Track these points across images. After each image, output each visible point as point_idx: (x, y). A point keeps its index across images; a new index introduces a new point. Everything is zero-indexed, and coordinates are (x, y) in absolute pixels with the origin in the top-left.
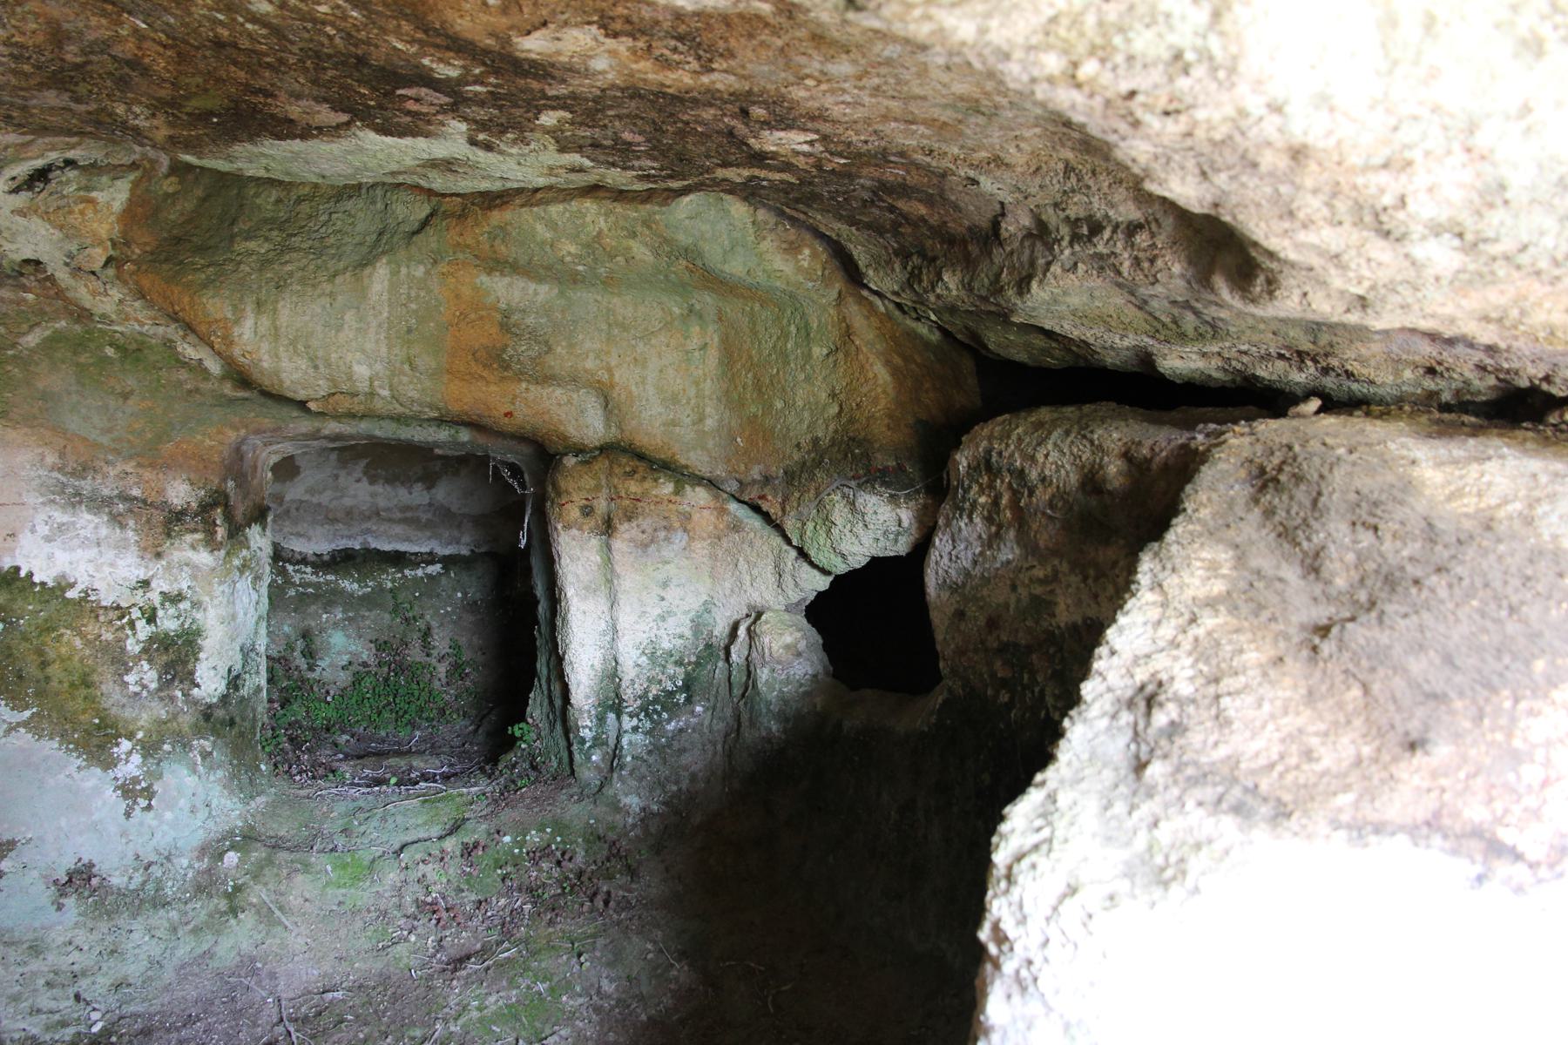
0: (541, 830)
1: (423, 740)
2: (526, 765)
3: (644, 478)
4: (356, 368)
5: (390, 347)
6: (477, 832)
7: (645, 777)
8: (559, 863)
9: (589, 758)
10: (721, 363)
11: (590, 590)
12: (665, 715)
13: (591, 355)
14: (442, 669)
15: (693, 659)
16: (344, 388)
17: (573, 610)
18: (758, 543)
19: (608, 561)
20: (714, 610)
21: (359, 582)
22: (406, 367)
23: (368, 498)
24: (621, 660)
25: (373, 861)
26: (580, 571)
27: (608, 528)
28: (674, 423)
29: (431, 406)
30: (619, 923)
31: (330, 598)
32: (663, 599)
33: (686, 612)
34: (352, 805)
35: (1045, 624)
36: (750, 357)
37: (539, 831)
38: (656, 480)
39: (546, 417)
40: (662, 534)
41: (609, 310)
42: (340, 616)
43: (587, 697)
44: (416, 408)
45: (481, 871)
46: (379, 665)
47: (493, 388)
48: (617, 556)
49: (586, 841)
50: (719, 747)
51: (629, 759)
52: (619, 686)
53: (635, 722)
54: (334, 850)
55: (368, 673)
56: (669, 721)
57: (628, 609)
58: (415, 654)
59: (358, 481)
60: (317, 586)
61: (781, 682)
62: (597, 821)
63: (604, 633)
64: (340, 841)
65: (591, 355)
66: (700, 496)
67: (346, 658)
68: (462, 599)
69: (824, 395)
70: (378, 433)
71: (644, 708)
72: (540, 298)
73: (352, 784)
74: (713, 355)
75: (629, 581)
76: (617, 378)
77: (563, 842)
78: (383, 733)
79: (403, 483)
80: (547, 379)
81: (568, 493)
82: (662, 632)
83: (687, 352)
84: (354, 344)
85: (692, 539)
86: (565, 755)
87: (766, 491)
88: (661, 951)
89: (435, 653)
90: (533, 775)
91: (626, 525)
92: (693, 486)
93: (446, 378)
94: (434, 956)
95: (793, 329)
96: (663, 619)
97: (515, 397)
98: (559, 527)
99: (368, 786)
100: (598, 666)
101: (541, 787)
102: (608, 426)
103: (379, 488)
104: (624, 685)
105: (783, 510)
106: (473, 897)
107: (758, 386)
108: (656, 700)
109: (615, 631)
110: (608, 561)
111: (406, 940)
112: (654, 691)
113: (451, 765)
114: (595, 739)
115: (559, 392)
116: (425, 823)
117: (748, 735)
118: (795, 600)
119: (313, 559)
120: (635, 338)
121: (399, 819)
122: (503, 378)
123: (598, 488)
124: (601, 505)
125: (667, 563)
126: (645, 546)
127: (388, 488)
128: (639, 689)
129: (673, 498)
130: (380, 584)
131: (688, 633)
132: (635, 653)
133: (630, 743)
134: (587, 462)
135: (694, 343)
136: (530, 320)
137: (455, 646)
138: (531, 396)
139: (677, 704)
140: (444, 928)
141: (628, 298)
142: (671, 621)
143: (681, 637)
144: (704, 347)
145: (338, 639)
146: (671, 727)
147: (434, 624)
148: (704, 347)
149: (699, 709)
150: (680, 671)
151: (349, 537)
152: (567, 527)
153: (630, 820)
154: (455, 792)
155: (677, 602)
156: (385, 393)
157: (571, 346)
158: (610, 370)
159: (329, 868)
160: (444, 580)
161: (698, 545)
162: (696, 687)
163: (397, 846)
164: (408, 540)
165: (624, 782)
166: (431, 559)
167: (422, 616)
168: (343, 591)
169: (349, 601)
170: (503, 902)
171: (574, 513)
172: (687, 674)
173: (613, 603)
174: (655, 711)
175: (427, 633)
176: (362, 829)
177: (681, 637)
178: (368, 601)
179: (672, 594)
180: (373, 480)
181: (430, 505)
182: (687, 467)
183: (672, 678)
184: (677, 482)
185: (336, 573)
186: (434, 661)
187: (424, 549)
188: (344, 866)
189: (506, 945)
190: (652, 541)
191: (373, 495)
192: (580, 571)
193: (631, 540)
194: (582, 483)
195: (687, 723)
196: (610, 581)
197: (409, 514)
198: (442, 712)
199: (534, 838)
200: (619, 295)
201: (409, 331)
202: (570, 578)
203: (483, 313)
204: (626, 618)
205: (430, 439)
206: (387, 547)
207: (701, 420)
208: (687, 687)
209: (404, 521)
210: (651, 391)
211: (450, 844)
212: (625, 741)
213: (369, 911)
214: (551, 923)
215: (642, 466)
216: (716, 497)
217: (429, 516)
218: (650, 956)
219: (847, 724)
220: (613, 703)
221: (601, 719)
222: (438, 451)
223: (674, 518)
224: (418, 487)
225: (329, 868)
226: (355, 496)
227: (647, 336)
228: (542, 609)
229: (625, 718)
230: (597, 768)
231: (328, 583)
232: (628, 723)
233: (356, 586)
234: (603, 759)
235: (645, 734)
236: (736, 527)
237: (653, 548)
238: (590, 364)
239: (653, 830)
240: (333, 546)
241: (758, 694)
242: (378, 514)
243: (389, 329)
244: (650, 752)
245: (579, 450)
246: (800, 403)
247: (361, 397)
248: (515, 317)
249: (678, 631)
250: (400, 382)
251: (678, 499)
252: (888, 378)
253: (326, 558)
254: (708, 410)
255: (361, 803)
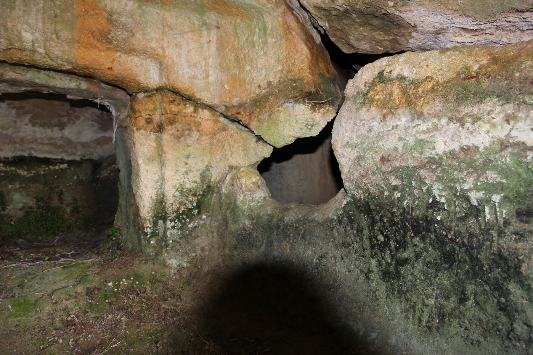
0: (128, 278)
1: (60, 240)
2: (115, 248)
3: (179, 104)
4: (24, 34)
5: (44, 24)
6: (95, 282)
7: (179, 250)
8: (138, 294)
9: (149, 243)
10: (218, 50)
11: (150, 160)
12: (188, 220)
13: (154, 41)
14: (68, 210)
15: (201, 193)
16: (17, 45)
17: (142, 170)
18: (235, 135)
19: (160, 147)
20: (211, 169)
21: (27, 171)
22: (54, 36)
23: (31, 133)
24: (166, 194)
25: (36, 301)
26: (145, 150)
27: (160, 128)
28: (194, 77)
29: (68, 61)
30: (174, 323)
31: (13, 178)
32: (187, 164)
33: (197, 171)
34: (24, 272)
35: (428, 154)
36: (234, 46)
37: (126, 279)
38: (185, 105)
39: (130, 72)
40: (187, 132)
41: (163, 18)
42: (18, 186)
43: (149, 213)
44: (60, 62)
45: (98, 301)
46: (38, 208)
47: (102, 54)
48: (164, 142)
49: (151, 283)
50: (215, 234)
51: (171, 242)
52: (165, 206)
53: (173, 224)
54: (14, 296)
55: (32, 211)
56: (190, 223)
57: (170, 168)
58: (55, 203)
59: (27, 124)
60: (6, 172)
61: (249, 201)
62: (156, 272)
63: (157, 181)
64: (17, 291)
65: (154, 41)
66: (205, 114)
67: (21, 205)
68: (77, 179)
69: (273, 61)
70: (37, 81)
71: (177, 217)
72: (128, 8)
73: (24, 261)
74: (213, 47)
75: (170, 155)
76: (167, 53)
77: (139, 284)
78: (40, 238)
79: (49, 127)
80: (131, 51)
81: (139, 111)
82: (186, 180)
83: (201, 44)
84: (22, 19)
85: (201, 135)
86: (136, 241)
87: (240, 110)
88: (198, 336)
89: (65, 202)
90: (119, 252)
91: (170, 127)
92: (202, 109)
93: (76, 45)
94: (73, 350)
95: (257, 30)
96: (187, 173)
97: (114, 60)
98: (135, 129)
99: (33, 262)
100: (154, 197)
101: (125, 258)
102: (161, 78)
103: (37, 129)
104: (167, 206)
105: (250, 119)
106: (93, 315)
107: (237, 60)
108: (184, 212)
109: (163, 179)
110: (160, 147)
111: (57, 342)
112: (182, 208)
113: (76, 251)
114: (152, 233)
115: (136, 59)
116: (65, 279)
117: (233, 227)
118: (253, 163)
119: (4, 160)
120: (176, 34)
121: (51, 278)
122: (109, 49)
123: (155, 109)
124: (157, 118)
125: (189, 146)
126: (179, 138)
127: (41, 129)
128: (175, 208)
129: (193, 114)
130: (38, 172)
131: (199, 181)
132: (173, 191)
133: (171, 234)
134: (150, 96)
135: (205, 40)
136: (123, 19)
137: (74, 199)
138: (122, 60)
139: (194, 214)
140: (78, 334)
141: (173, 13)
142: (191, 175)
143: (195, 182)
144: (209, 42)
145: (17, 197)
146: (191, 226)
147: (64, 190)
148: (209, 42)
149: (204, 217)
150: (195, 199)
151: (22, 151)
152: (139, 129)
153: (172, 271)
154: (80, 262)
155: (194, 165)
156: (42, 51)
157: (144, 34)
158: (163, 49)
159: (10, 307)
160: (68, 171)
161: (204, 138)
162: (202, 206)
163: (50, 291)
164: (51, 153)
165: (168, 253)
166: (62, 161)
167: (58, 186)
168: (19, 175)
169: (22, 179)
170: (110, 316)
171: (142, 122)
172: (198, 200)
173: (162, 165)
174: (183, 218)
175: (61, 193)
176: (30, 284)
177: (195, 182)
178: (33, 179)
179: (191, 161)
180: (34, 125)
181: (62, 137)
182: (200, 99)
183: (191, 202)
184: (195, 106)
185: (15, 166)
186: (64, 206)
187: (59, 157)
188: (20, 305)
189: (114, 340)
190: (182, 136)
191: (34, 132)
192: (145, 150)
193: (173, 135)
194: (147, 107)
195: (198, 224)
196: (160, 156)
197: (52, 141)
198: (69, 228)
199: (124, 282)
200: (169, 11)
201: (56, 16)
202: (140, 154)
203: (98, 12)
204: (169, 173)
205: (66, 86)
206: (41, 156)
207: (207, 77)
208: (198, 206)
209: (49, 144)
210: (183, 61)
211: (80, 289)
212: (168, 233)
213: (34, 328)
214: (139, 326)
215: (178, 98)
216: (214, 115)
217: (61, 142)
218: (192, 339)
219: (286, 219)
220: (160, 215)
221: (155, 223)
222: (69, 97)
223: (193, 125)
224: (56, 129)
225: (10, 307)
226: (25, 132)
227: (182, 34)
228: (123, 174)
229: (168, 222)
230: (154, 247)
231: (12, 171)
232: (169, 224)
233: (26, 173)
234: (156, 243)
235: (178, 229)
236: (224, 129)
237: (182, 139)
238: (153, 45)
239: (184, 276)
240: (14, 154)
241: (238, 207)
242: (36, 141)
243: (44, 13)
244: (181, 238)
245: (146, 90)
246: (260, 66)
247: (27, 52)
248: (115, 17)
249: (194, 179)
250: (50, 45)
251: (195, 115)
252: (308, 51)
253: (11, 159)
254: (210, 72)
255: (29, 270)
